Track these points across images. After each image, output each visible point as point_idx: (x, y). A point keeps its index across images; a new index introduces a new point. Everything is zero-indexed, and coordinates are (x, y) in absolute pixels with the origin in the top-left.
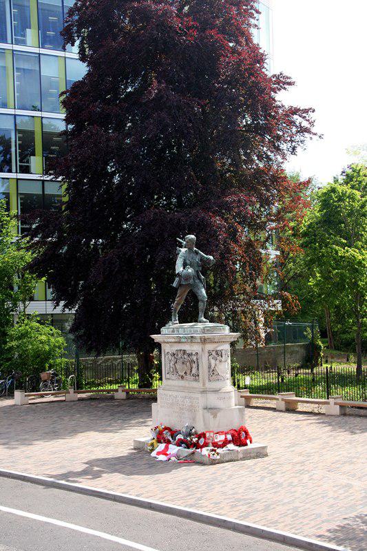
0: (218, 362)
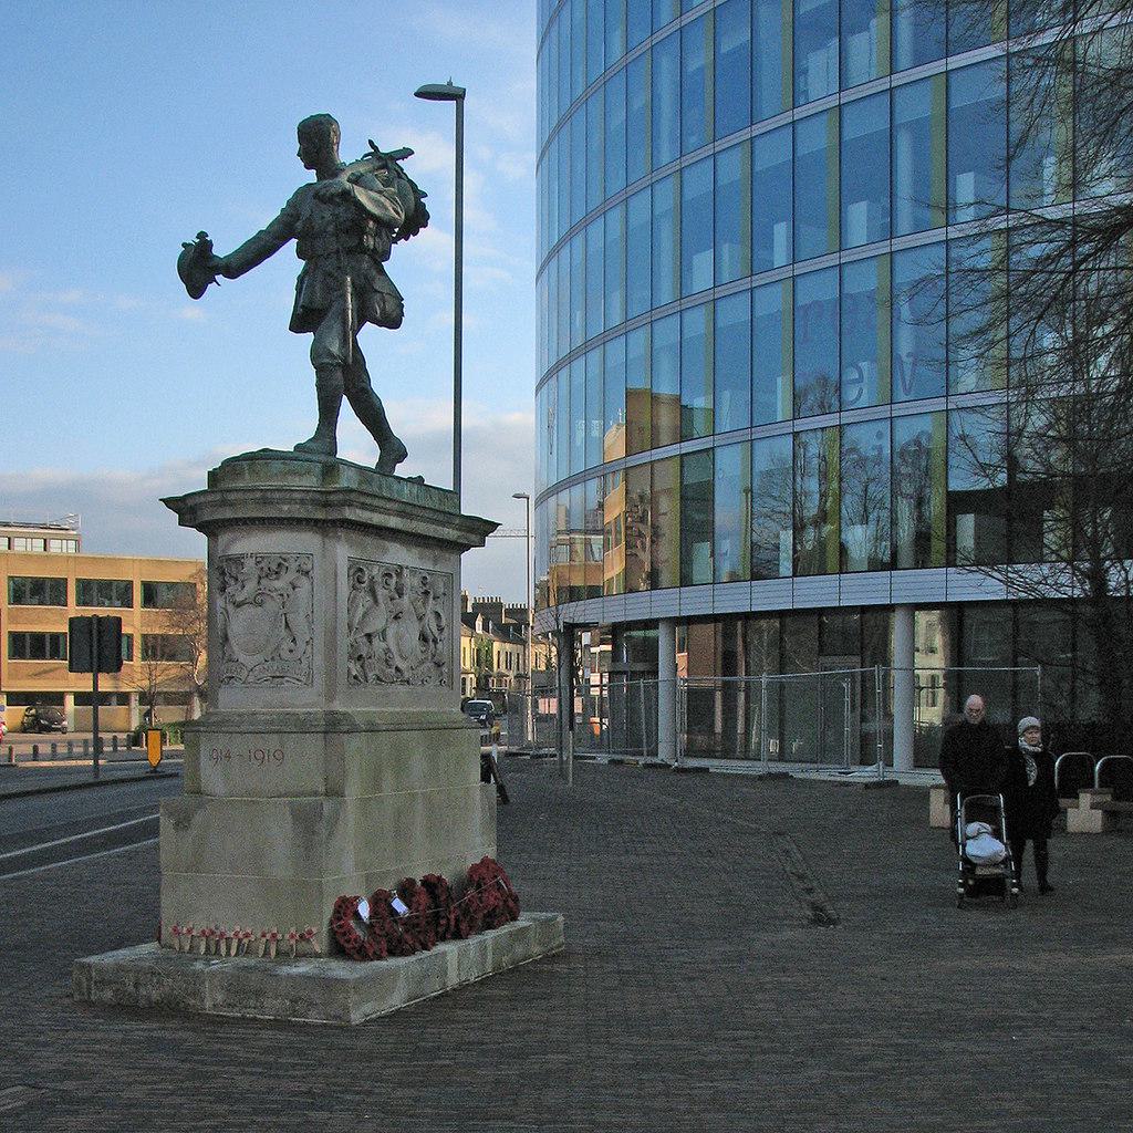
0: (230, 608)
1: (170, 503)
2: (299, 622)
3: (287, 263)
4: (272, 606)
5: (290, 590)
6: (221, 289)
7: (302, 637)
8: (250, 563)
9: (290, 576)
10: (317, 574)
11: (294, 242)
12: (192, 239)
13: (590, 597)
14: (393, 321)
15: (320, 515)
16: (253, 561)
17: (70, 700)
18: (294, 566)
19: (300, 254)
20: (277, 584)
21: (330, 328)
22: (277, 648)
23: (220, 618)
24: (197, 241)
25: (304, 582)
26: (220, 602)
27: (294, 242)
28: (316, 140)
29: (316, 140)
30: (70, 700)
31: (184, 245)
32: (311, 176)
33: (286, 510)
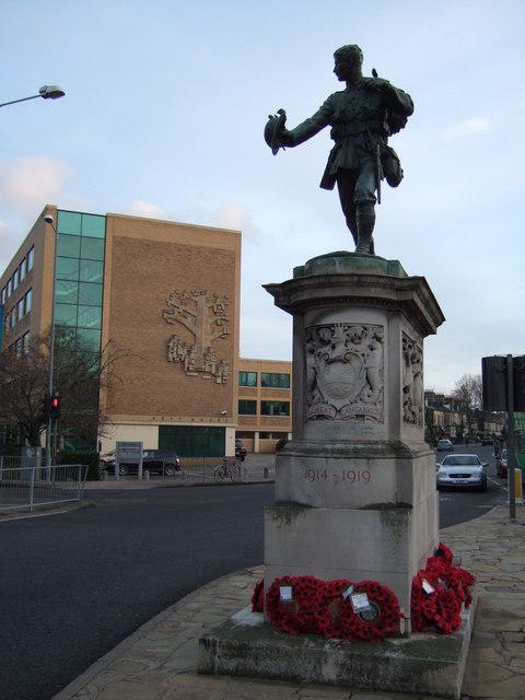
0: (322, 364)
1: (270, 288)
2: (375, 374)
3: (324, 142)
4: (355, 363)
5: (369, 351)
6: (285, 152)
7: (378, 385)
8: (339, 331)
9: (367, 342)
10: (385, 340)
11: (328, 129)
12: (274, 113)
13: (276, 412)
14: (395, 180)
15: (393, 297)
16: (341, 329)
17: (257, 436)
18: (371, 333)
19: (333, 136)
20: (358, 347)
21: (368, 178)
22: (359, 395)
23: (310, 373)
24: (279, 116)
25: (378, 345)
26: (311, 360)
27: (328, 129)
28: (347, 61)
29: (347, 61)
30: (257, 436)
31: (270, 117)
32: (342, 86)
33: (373, 292)
